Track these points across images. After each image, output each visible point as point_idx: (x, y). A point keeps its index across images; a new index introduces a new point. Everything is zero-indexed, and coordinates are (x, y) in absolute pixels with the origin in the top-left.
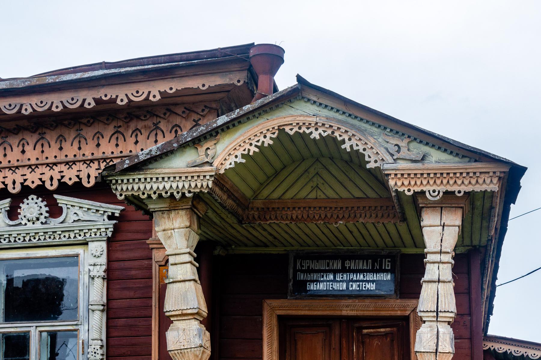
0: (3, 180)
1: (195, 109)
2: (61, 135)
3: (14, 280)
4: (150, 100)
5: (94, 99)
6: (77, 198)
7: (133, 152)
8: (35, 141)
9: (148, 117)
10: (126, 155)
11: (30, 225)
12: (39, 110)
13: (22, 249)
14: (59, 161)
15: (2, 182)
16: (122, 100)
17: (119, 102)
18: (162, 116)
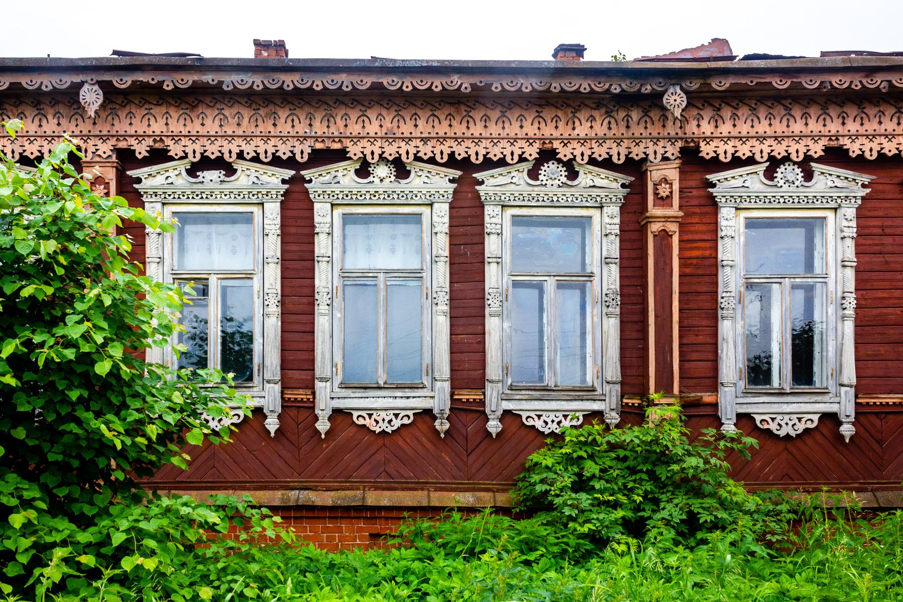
0: (2, 148)
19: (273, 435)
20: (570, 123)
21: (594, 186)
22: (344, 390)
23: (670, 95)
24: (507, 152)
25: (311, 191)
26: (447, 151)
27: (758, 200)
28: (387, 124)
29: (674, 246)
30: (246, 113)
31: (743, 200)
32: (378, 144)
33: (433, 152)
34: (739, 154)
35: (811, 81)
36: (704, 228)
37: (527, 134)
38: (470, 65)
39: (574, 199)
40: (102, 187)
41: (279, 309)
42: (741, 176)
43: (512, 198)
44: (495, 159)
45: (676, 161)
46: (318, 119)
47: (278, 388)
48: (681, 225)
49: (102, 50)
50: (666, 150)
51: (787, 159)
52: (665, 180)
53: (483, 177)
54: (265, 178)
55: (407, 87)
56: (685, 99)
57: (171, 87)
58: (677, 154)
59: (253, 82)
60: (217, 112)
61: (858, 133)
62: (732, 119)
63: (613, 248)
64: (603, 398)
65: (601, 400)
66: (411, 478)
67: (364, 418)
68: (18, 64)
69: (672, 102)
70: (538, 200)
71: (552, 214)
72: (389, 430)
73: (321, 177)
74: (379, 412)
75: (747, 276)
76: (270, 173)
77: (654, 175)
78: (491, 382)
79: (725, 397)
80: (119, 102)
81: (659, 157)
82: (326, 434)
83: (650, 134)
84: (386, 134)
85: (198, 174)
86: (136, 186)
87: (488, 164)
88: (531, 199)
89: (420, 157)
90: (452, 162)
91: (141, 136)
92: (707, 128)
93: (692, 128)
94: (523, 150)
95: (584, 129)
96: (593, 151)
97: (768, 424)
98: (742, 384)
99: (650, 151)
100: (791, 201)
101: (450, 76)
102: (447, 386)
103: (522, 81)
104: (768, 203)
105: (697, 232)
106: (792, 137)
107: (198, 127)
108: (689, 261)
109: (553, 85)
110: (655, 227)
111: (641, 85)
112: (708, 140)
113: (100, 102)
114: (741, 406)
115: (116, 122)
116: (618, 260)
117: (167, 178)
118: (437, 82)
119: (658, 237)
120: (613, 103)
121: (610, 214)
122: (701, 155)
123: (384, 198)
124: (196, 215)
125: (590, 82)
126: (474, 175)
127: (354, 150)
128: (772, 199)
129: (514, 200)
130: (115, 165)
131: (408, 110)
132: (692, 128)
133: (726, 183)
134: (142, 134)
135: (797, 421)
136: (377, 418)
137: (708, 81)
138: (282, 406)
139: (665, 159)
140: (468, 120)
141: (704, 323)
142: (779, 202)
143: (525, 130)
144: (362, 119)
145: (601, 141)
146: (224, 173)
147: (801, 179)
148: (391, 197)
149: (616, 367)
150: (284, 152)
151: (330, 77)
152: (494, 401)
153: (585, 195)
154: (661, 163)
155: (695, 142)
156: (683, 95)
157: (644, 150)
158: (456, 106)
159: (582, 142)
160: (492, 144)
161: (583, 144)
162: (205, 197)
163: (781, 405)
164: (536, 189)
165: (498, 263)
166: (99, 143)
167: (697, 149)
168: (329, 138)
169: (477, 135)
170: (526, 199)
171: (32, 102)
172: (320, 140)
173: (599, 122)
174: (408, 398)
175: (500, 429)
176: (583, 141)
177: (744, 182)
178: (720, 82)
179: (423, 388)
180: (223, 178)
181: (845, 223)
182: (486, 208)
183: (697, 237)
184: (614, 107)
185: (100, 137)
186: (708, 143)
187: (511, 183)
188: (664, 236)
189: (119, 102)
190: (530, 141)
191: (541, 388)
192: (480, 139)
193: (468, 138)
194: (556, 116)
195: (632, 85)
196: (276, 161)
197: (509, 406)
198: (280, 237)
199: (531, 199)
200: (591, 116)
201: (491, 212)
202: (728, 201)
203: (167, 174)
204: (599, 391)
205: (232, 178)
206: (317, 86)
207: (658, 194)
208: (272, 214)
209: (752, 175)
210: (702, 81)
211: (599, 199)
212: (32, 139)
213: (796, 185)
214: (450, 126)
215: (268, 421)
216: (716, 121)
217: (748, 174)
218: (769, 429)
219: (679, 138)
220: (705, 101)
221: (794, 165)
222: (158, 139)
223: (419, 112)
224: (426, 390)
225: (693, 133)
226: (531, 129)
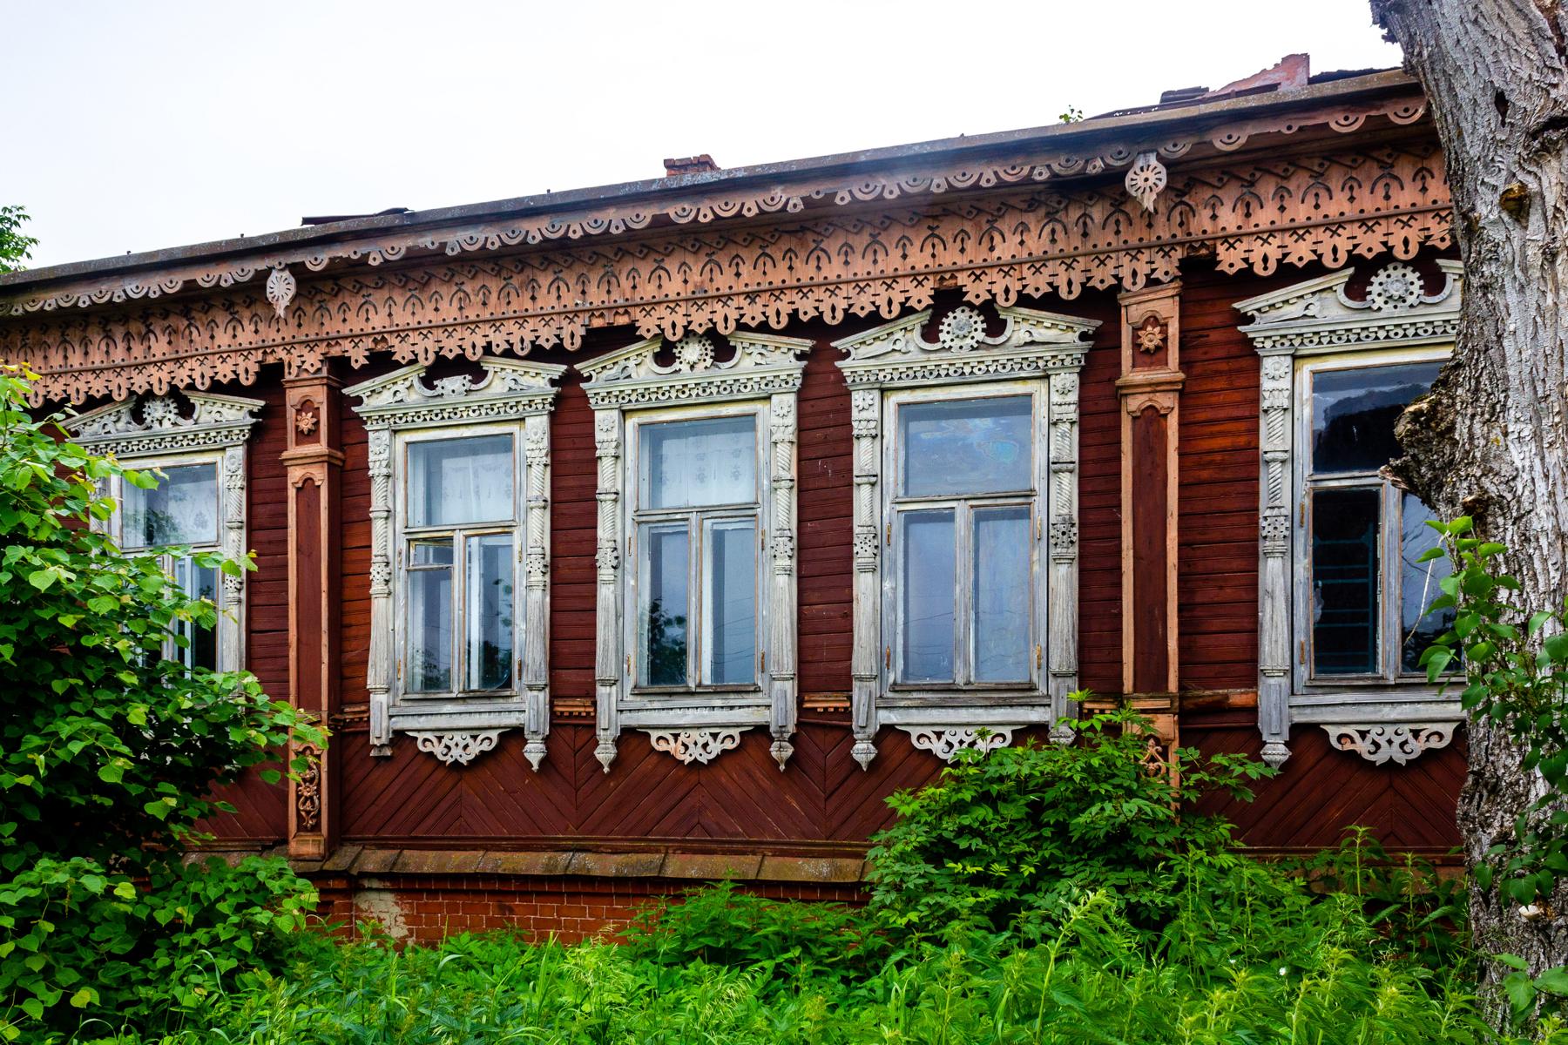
3: (750, 434)
5: (802, 199)
7: (1347, 214)
11: (1388, 309)
12: (171, 291)
16: (493, 244)
19: (535, 767)
20: (986, 240)
21: (1033, 343)
22: (639, 698)
23: (1138, 171)
24: (882, 302)
25: (590, 393)
26: (786, 309)
27: (1335, 339)
28: (695, 277)
29: (1170, 433)
30: (494, 285)
31: (1306, 341)
32: (681, 310)
33: (764, 313)
34: (1292, 259)
35: (964, 175)
36: (1237, 396)
37: (913, 268)
38: (794, 168)
39: (1000, 368)
40: (310, 414)
41: (547, 578)
42: (1302, 297)
43: (896, 375)
44: (862, 314)
45: (1172, 285)
46: (594, 283)
47: (543, 697)
48: (1182, 394)
49: (285, 220)
50: (1154, 266)
51: (1386, 259)
52: (1154, 320)
53: (848, 346)
54: (526, 381)
55: (705, 216)
56: (1164, 176)
57: (379, 260)
58: (1174, 271)
59: (487, 239)
60: (455, 289)
61: (1274, 227)
62: (1277, 199)
63: (1067, 444)
64: (1046, 701)
65: (1044, 705)
66: (738, 834)
67: (667, 741)
68: (188, 255)
69: (1140, 182)
70: (1348, 341)
71: (965, 396)
72: (704, 759)
73: (605, 371)
74: (689, 732)
75: (1315, 477)
76: (533, 372)
77: (1134, 313)
78: (861, 679)
79: (1269, 696)
80: (328, 290)
81: (1141, 280)
82: (611, 765)
83: (1125, 242)
84: (693, 293)
85: (435, 383)
86: (355, 409)
87: (853, 323)
88: (927, 374)
89: (746, 324)
90: (795, 327)
91: (357, 336)
92: (1229, 219)
93: (1202, 223)
94: (907, 295)
95: (1009, 247)
96: (1024, 282)
97: (1353, 742)
98: (1304, 672)
99: (1125, 273)
100: (1401, 333)
101: (769, 190)
102: (790, 688)
103: (884, 182)
104: (1357, 341)
105: (1222, 406)
106: (1395, 215)
107: (431, 315)
108: (1209, 458)
109: (936, 181)
110: (1134, 403)
111: (1087, 162)
112: (1231, 241)
113: (291, 294)
114: (1301, 710)
115: (326, 321)
116: (1077, 465)
117: (395, 393)
118: (750, 203)
119: (1141, 421)
120: (1056, 198)
121: (1059, 387)
122: (1218, 268)
123: (698, 395)
124: (435, 444)
125: (996, 168)
126: (833, 344)
127: (647, 325)
128: (1363, 335)
129: (900, 378)
130: (325, 381)
131: (726, 251)
132: (1202, 223)
133: (1274, 313)
134: (359, 332)
135: (1410, 736)
136: (687, 741)
137: (1207, 138)
138: (552, 725)
139: (1152, 282)
140: (818, 254)
141: (1235, 564)
142: (1377, 338)
143: (910, 261)
144: (657, 273)
145: (1037, 264)
146: (470, 378)
147: (1416, 289)
148: (708, 391)
149: (1068, 648)
150: (547, 339)
151: (592, 216)
152: (864, 710)
153: (1018, 359)
154: (1144, 290)
155: (1207, 247)
156: (1161, 168)
157: (1114, 272)
158: (800, 234)
159: (1006, 269)
160: (858, 289)
161: (1007, 273)
162: (448, 414)
163: (1378, 707)
164: (933, 356)
165: (873, 485)
166: (305, 351)
167: (1213, 259)
168: (610, 309)
169: (832, 278)
170: (919, 375)
171: (224, 305)
172: (597, 313)
173: (1034, 232)
174: (732, 708)
175: (872, 756)
176: (1007, 268)
177: (1307, 308)
178: (1230, 137)
179: (755, 691)
180: (468, 385)
181: (780, 421)
182: (855, 395)
183: (1222, 414)
184: (1059, 203)
185: (306, 343)
186: (1232, 246)
187: (894, 350)
188: (1151, 419)
189: (328, 290)
190: (917, 277)
191: (942, 687)
192: (837, 285)
193: (819, 285)
194: (962, 231)
195: (1070, 164)
196: (538, 354)
197: (889, 718)
198: (549, 469)
199: (927, 374)
200: (846, 244)
201: (860, 402)
202: (1278, 345)
203: (395, 388)
204: (1042, 690)
205: (481, 385)
206: (574, 232)
207: (1141, 345)
208: (536, 434)
209: (1324, 295)
210: (1195, 140)
211: (1041, 363)
212: (225, 355)
213: (1408, 303)
214: (791, 268)
215: (528, 747)
216: (1248, 205)
217: (1313, 293)
218: (1353, 752)
219: (1178, 244)
220: (1223, 173)
221: (1404, 267)
222: (379, 338)
223: (744, 253)
224: (760, 695)
225: (1205, 232)
226: (919, 259)
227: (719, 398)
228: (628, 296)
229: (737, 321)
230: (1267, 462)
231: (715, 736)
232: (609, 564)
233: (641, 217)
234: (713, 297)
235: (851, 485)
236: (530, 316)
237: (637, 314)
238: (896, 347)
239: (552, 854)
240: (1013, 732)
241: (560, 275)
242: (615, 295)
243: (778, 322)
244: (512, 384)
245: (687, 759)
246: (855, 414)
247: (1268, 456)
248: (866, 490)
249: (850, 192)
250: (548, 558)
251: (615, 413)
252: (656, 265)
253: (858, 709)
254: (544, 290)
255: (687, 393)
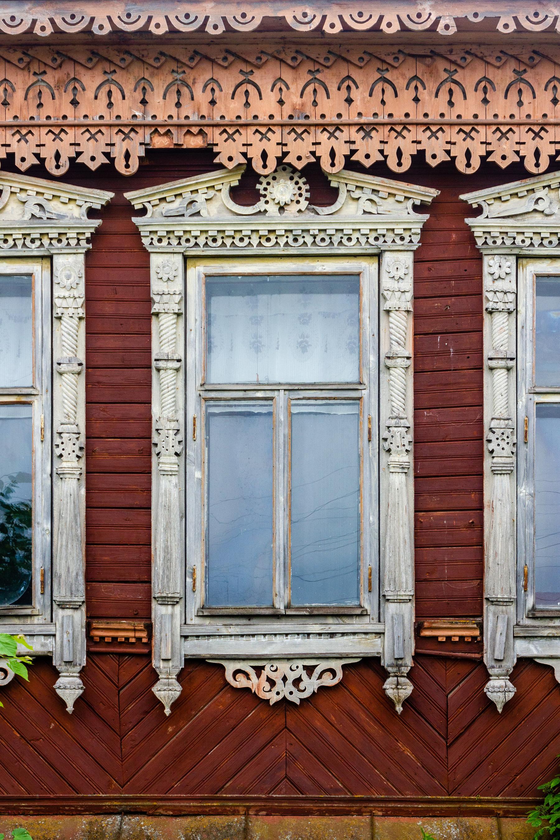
1: (349, 58)
2: (349, 77)
4: (207, 32)
5: (456, 20)
6: (417, 184)
8: (301, 84)
9: (468, 60)
10: (126, 122)
13: (228, 259)
14: (344, 122)
15: (104, 153)
16: (43, 29)
17: (500, 27)
18: (50, 62)
19: (70, 708)
22: (207, 621)
24: (527, 151)
25: (144, 231)
26: (409, 150)
27: (28, 242)
32: (276, 137)
41: (82, 464)
43: (537, 240)
44: (503, 165)
46: (159, 91)
53: (480, 201)
54: (55, 207)
59: (34, 22)
66: (337, 790)
67: (247, 675)
72: (296, 698)
73: (164, 204)
74: (276, 664)
76: (65, 197)
78: (494, 602)
82: (173, 707)
89: (358, 163)
118: (390, 16)
129: (541, 244)
131: (334, 70)
136: (273, 676)
144: (243, 88)
148: (301, 241)
152: (500, 639)
158: (428, 61)
160: (498, 134)
165: (509, 369)
169: (468, 117)
172: (162, 130)
174: (332, 635)
175: (511, 695)
177: (536, 202)
179: (361, 615)
187: (535, 211)
192: (474, 127)
193: (451, 125)
197: (528, 650)
198: (83, 323)
201: (495, 269)
208: (68, 277)
214: (416, 100)
223: (356, 74)
224: (366, 619)
227: (314, 250)
228: (204, 112)
229: (347, 158)
230: (491, 369)
231: (310, 670)
232: (172, 451)
233: (249, 18)
234: (316, 125)
235: (480, 368)
236: (140, 126)
237: (215, 136)
238: (538, 208)
239: (93, 818)
240: (344, 667)
241: (318, 76)
242: (187, 109)
243: (400, 164)
244: (37, 212)
245: (274, 698)
246: (487, 282)
247: (493, 364)
248: (500, 376)
249: (515, 19)
250: (83, 439)
251: (179, 259)
252: (242, 78)
253: (494, 639)
254: (90, 94)
255: (274, 241)
